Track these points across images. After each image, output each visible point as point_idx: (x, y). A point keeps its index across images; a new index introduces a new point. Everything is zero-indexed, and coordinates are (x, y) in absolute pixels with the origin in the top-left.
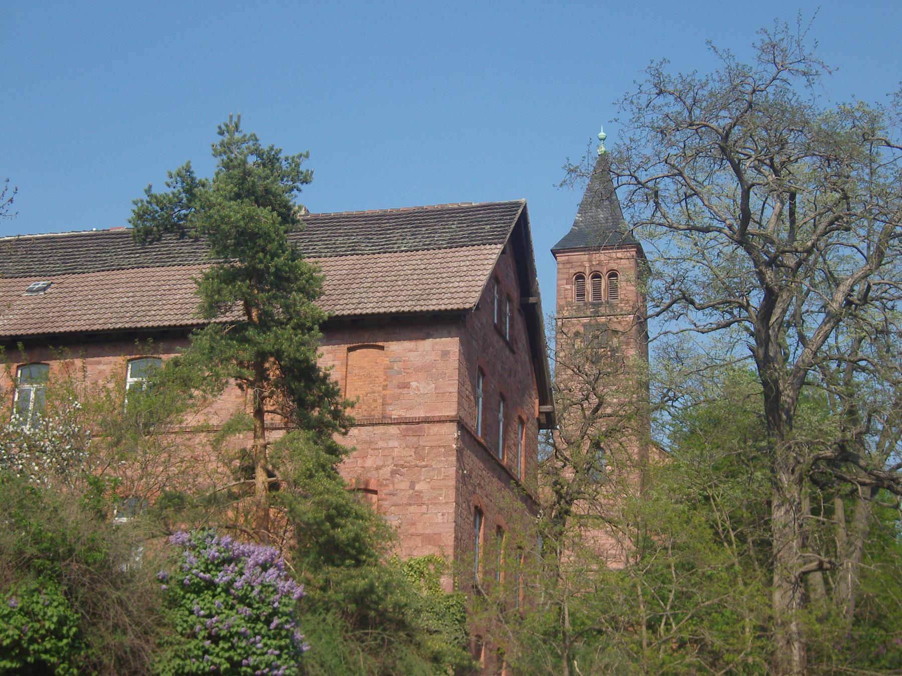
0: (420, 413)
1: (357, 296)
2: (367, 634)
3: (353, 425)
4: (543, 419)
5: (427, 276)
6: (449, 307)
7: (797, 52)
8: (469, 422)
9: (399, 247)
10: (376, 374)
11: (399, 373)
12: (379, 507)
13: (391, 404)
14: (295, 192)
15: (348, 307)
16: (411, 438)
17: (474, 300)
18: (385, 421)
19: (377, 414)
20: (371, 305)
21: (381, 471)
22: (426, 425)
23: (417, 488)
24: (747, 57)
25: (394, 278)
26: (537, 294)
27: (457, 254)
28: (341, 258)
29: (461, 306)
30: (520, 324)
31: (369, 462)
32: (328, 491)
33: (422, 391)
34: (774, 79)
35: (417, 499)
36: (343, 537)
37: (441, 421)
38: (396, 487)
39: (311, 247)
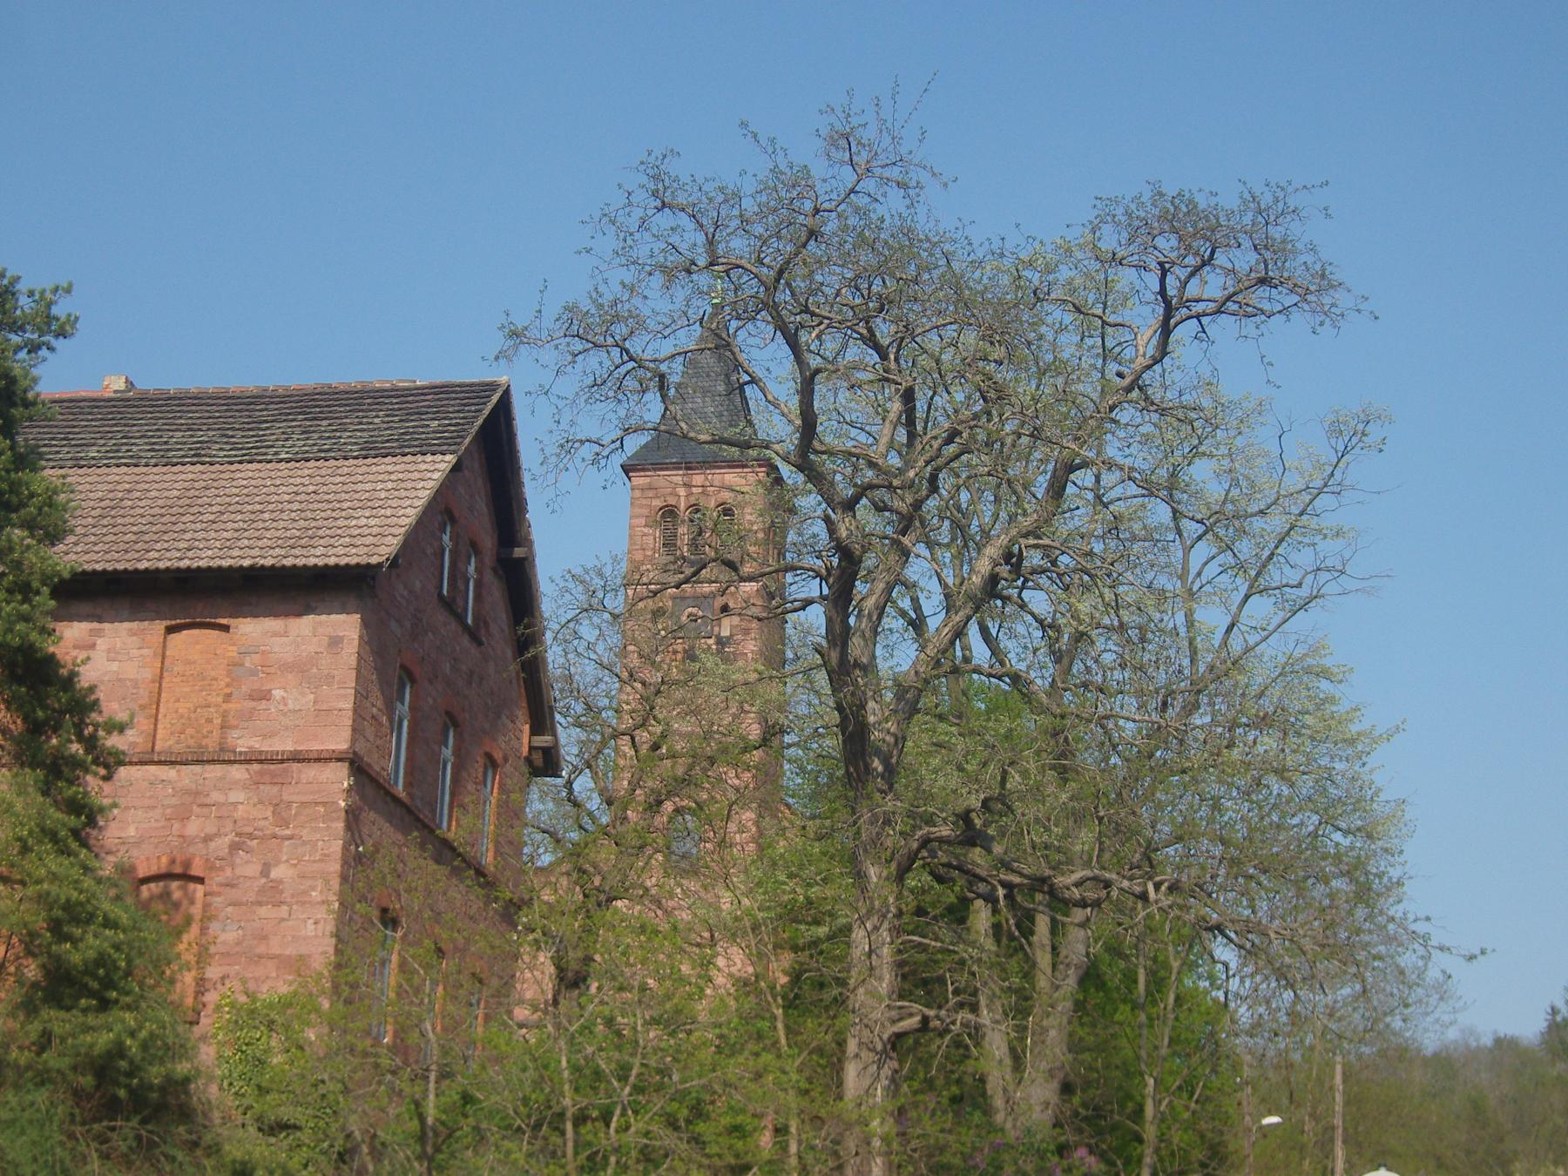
0: (286, 745)
1: (188, 536)
2: (113, 1129)
3: (121, 763)
4: (538, 759)
5: (316, 506)
6: (343, 561)
7: (891, 148)
8: (374, 761)
9: (276, 453)
10: (213, 673)
11: (254, 673)
12: (206, 906)
13: (236, 727)
14: (44, 352)
15: (168, 555)
16: (268, 787)
17: (388, 550)
18: (224, 757)
19: (211, 744)
20: (210, 553)
21: (212, 845)
22: (295, 765)
23: (273, 875)
24: (807, 152)
25: (258, 507)
26: (528, 543)
27: (374, 469)
28: (175, 469)
29: (364, 560)
30: (496, 593)
31: (193, 828)
32: (54, 877)
33: (291, 706)
34: (852, 191)
35: (272, 893)
36: (76, 958)
37: (321, 759)
38: (238, 871)
39: (124, 448)
